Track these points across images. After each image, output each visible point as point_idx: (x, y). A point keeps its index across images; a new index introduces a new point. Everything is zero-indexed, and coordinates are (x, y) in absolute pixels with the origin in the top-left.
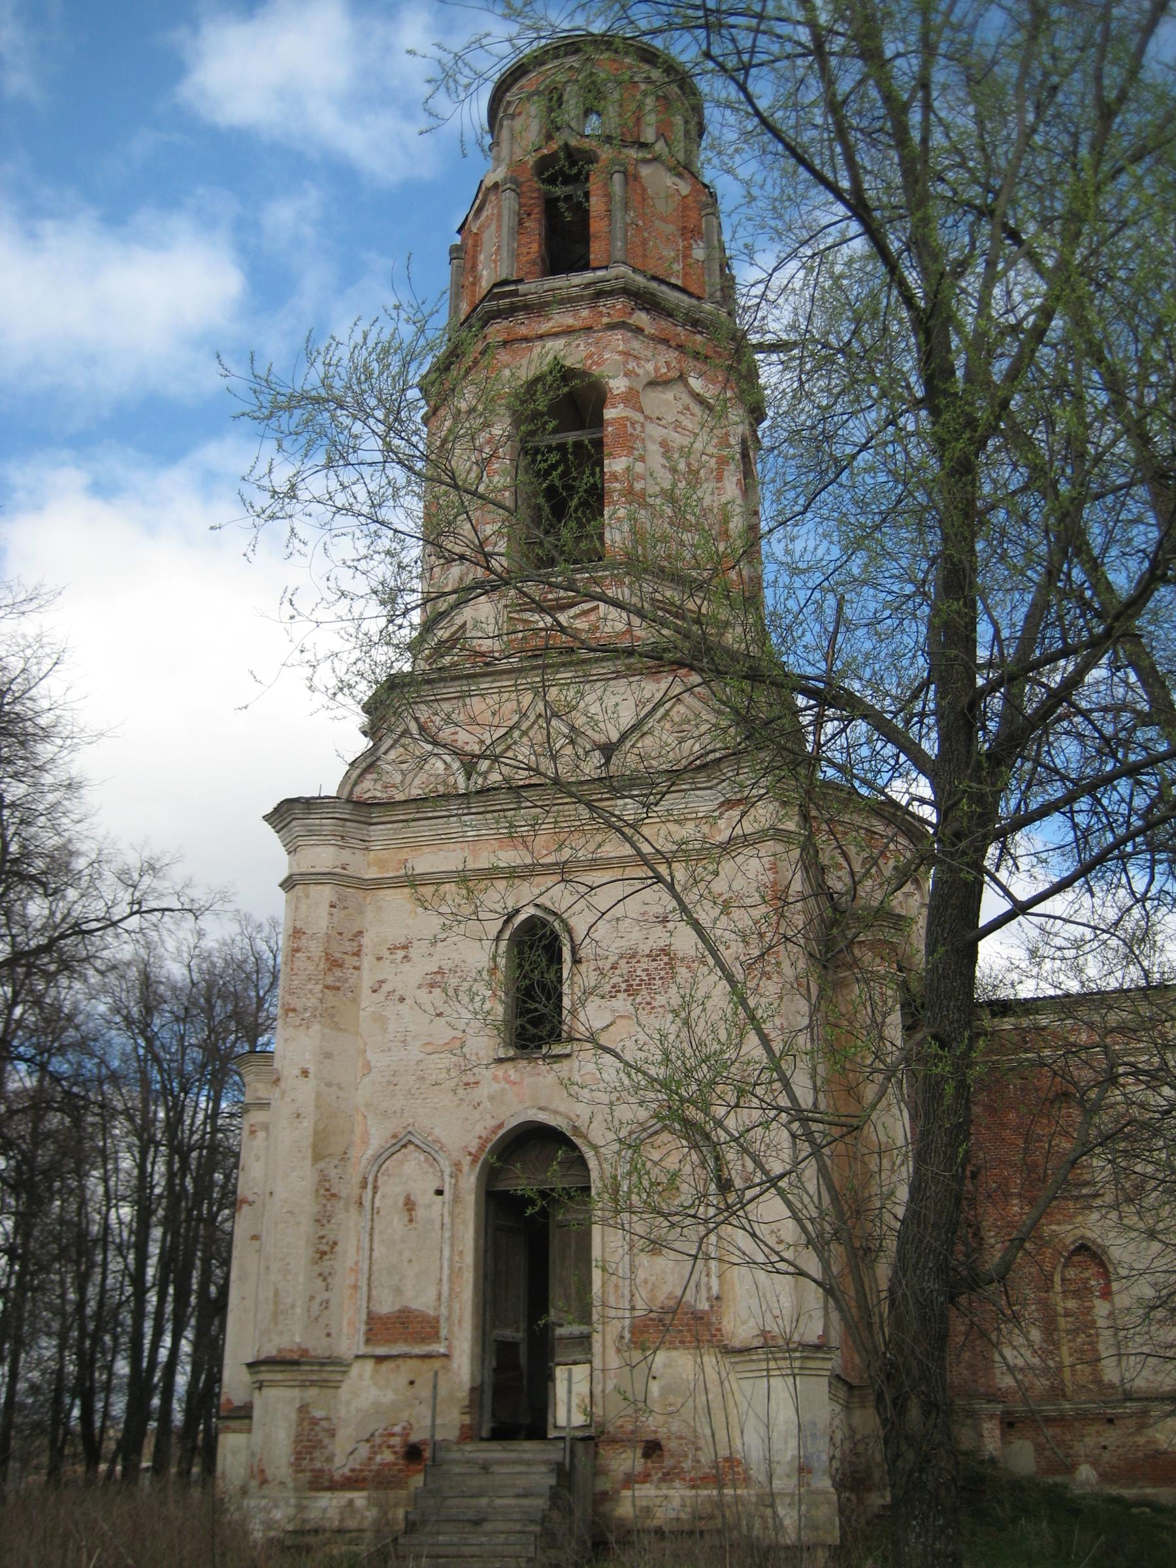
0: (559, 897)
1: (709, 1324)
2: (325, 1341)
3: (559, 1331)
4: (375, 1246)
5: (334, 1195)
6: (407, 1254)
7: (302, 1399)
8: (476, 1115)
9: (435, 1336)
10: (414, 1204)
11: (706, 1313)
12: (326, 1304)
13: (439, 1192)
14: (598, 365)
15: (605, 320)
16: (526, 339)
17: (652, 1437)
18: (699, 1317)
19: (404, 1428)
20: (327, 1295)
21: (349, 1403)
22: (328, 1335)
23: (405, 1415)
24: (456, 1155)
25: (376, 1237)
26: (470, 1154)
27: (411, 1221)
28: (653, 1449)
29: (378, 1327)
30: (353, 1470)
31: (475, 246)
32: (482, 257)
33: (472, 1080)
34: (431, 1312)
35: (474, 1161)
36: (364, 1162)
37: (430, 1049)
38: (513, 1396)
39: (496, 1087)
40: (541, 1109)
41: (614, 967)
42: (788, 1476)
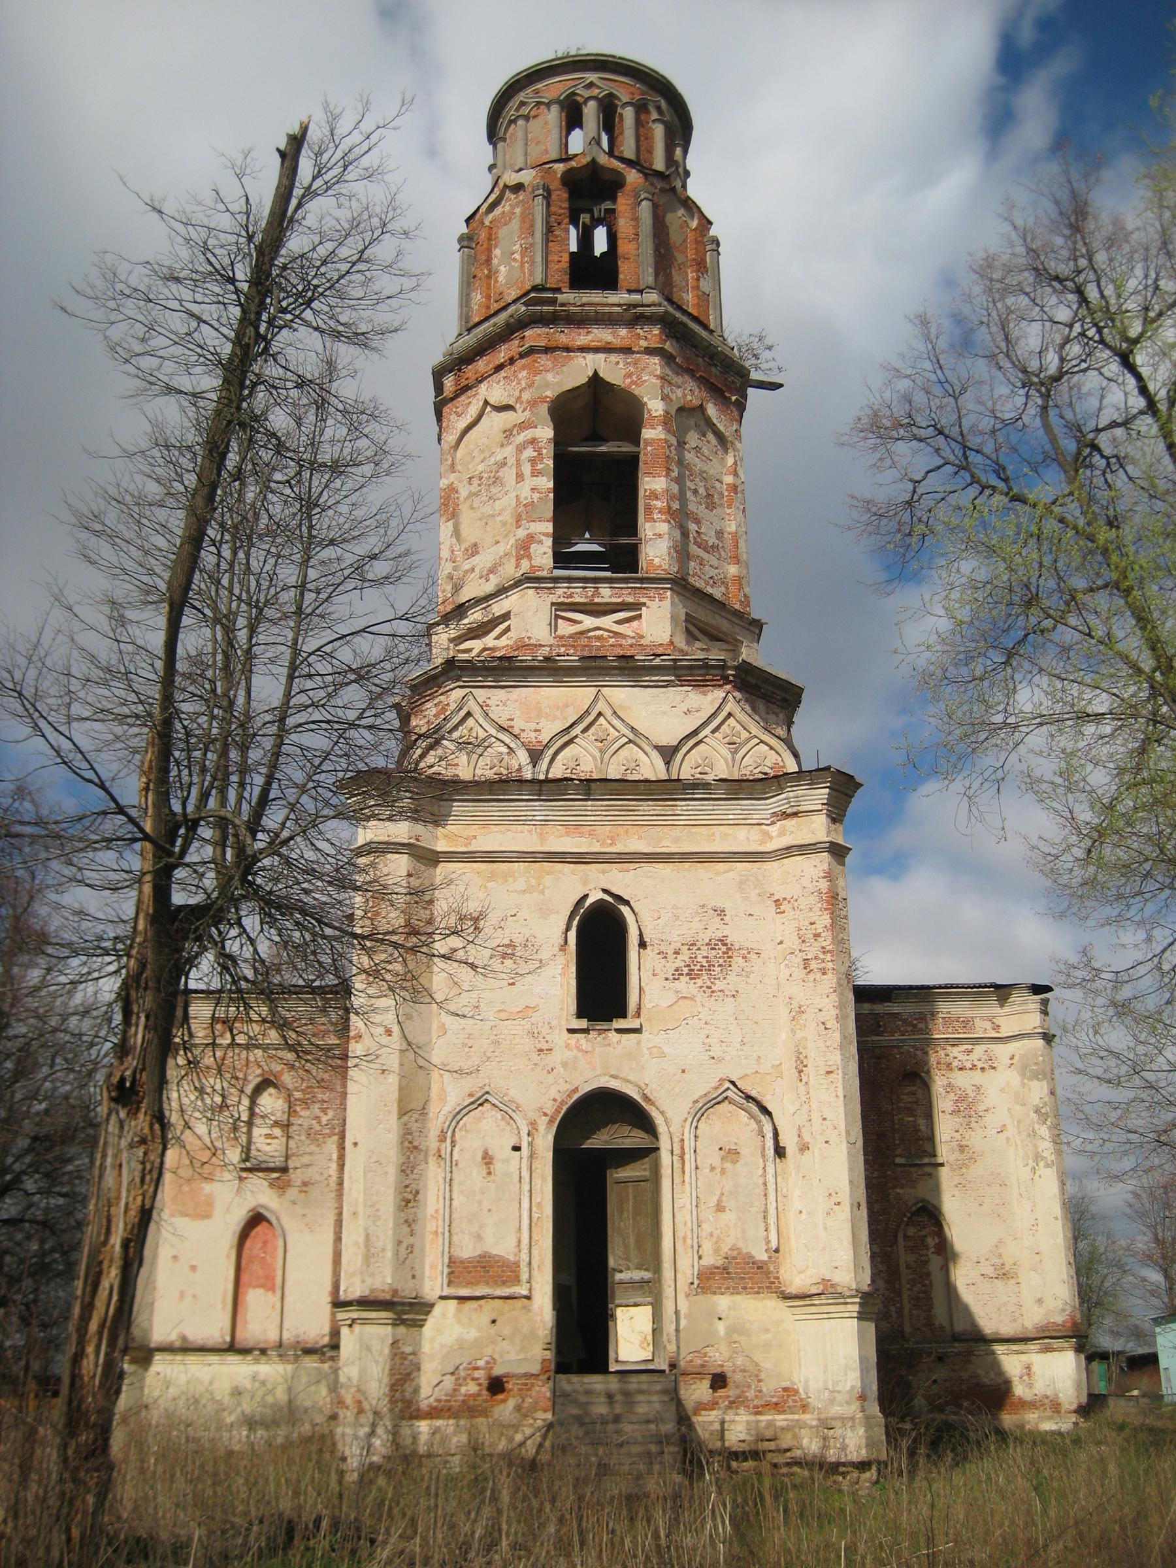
0: (619, 880)
1: (768, 1273)
2: (411, 1283)
3: (618, 1277)
4: (455, 1196)
5: (416, 1148)
6: (486, 1205)
7: (394, 1335)
8: (550, 1079)
9: (516, 1280)
10: (492, 1158)
11: (766, 1263)
12: (411, 1248)
13: (517, 1149)
14: (638, 385)
15: (643, 343)
16: (567, 349)
17: (719, 1370)
18: (760, 1267)
19: (488, 1363)
20: (411, 1240)
21: (432, 1340)
22: (414, 1277)
23: (489, 1351)
24: (532, 1115)
25: (455, 1187)
26: (545, 1115)
27: (489, 1173)
28: (719, 1381)
29: (457, 1270)
30: (439, 1401)
31: (489, 239)
32: (497, 252)
33: (545, 1047)
34: (512, 1258)
35: (551, 1121)
36: (441, 1118)
37: (503, 1016)
38: (582, 1333)
39: (568, 1054)
40: (612, 1076)
41: (677, 953)
42: (848, 1403)
